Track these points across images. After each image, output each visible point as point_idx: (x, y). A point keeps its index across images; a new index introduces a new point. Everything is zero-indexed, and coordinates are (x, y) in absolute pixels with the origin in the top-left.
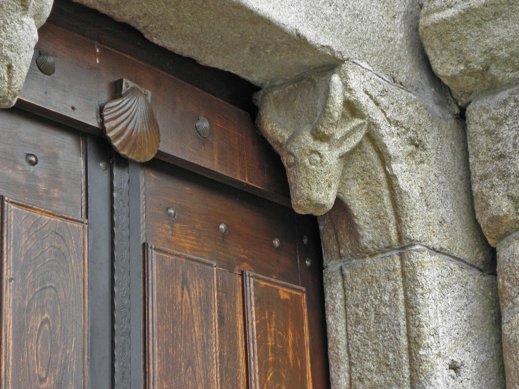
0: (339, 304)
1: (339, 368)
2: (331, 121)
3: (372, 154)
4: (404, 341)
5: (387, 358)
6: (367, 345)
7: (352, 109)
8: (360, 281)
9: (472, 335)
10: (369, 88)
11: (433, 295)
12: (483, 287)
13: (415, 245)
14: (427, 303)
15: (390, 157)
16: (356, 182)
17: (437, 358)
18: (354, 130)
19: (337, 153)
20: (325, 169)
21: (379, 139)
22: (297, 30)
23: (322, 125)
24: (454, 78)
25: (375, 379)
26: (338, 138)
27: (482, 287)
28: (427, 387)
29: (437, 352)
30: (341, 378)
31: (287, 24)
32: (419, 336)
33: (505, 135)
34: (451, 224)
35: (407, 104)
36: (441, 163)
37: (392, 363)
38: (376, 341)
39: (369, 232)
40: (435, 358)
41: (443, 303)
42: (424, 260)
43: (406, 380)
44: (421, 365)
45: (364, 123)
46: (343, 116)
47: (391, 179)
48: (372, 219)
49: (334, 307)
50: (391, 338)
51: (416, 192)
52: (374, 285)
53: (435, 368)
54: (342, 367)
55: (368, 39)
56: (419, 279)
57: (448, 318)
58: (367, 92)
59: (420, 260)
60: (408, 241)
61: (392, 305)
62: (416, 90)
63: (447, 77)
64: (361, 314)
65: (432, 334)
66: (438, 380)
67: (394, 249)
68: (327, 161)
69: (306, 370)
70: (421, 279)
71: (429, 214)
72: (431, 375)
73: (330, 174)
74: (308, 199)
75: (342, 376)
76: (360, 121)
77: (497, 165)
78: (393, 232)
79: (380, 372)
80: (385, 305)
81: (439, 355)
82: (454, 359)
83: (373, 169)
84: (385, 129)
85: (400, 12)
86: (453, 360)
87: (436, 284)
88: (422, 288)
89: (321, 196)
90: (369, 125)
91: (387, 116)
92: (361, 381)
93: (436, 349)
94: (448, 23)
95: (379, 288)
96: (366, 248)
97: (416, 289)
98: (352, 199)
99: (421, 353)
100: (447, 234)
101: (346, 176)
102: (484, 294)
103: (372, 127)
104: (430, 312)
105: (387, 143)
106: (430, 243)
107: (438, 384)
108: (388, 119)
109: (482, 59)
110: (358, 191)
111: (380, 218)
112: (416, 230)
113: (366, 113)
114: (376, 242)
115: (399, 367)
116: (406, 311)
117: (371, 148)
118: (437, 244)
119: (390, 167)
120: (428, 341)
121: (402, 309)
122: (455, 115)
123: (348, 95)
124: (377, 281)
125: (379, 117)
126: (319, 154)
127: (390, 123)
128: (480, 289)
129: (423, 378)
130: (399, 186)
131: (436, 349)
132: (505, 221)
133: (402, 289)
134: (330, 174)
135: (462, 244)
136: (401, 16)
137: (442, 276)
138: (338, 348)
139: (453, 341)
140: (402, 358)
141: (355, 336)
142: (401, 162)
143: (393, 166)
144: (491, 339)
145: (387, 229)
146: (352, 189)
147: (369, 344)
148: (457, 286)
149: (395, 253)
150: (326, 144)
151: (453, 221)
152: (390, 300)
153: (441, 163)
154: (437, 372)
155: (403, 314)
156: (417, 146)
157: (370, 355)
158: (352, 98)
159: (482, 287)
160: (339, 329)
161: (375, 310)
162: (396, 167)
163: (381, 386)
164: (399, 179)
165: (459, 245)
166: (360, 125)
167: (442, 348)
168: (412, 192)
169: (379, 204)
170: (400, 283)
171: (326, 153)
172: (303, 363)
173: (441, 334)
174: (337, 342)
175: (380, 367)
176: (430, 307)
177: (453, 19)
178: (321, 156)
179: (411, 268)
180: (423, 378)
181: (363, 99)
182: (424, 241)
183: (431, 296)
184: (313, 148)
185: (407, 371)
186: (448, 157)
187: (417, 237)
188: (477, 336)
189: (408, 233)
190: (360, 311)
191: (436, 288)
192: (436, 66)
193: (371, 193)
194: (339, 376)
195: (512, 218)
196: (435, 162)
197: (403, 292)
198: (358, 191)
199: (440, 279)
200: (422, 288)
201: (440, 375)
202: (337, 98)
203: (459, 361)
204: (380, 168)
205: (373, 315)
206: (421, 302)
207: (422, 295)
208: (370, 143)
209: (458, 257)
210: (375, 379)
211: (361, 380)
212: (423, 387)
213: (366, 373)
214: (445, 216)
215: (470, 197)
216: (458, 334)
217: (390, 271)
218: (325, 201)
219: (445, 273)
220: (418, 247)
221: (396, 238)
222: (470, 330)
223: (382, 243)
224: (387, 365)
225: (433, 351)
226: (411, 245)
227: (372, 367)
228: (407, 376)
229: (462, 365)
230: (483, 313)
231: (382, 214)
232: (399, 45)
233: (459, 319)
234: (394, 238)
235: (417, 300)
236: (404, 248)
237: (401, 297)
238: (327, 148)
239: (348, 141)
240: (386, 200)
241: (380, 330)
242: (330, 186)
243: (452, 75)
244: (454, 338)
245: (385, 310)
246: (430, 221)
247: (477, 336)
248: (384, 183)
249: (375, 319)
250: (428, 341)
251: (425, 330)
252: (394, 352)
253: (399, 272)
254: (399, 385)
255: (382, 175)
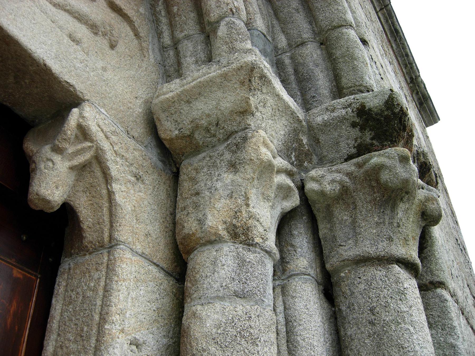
0: (62, 289)
1: (50, 337)
2: (65, 137)
3: (99, 174)
4: (97, 317)
5: (82, 330)
6: (72, 320)
7: (84, 133)
8: (79, 272)
9: (158, 322)
10: (101, 123)
11: (127, 284)
12: (176, 290)
13: (120, 245)
14: (119, 288)
15: (112, 178)
16: (85, 195)
17: (120, 333)
18: (83, 150)
19: (67, 164)
20: (55, 173)
21: (104, 162)
22: (44, 60)
23: (58, 140)
24: (171, 140)
25: (71, 347)
26: (70, 152)
27: (174, 290)
28: (105, 355)
29: (120, 328)
30: (50, 346)
31: (35, 51)
32: (107, 313)
33: (201, 179)
34: (156, 239)
35: (134, 149)
36: (156, 197)
37: (85, 335)
38: (78, 317)
39: (90, 235)
40: (118, 333)
41: (135, 292)
42: (124, 256)
43: (91, 348)
44: (104, 337)
45: (93, 146)
46: (77, 137)
47: (110, 194)
48: (93, 224)
49: (58, 291)
50: (88, 315)
51: (129, 208)
52: (87, 275)
53: (114, 340)
54: (52, 337)
55: (110, 98)
56: (117, 269)
57: (137, 305)
58: (99, 126)
59: (121, 255)
60: (115, 241)
61: (95, 290)
62: (145, 147)
63: (167, 139)
64: (73, 296)
65: (118, 312)
66: (116, 351)
67: (106, 248)
68: (57, 168)
69: (22, 335)
70: (119, 270)
71: (137, 226)
72: (111, 345)
73: (59, 179)
74: (37, 194)
75: (51, 344)
76: (89, 144)
77: (193, 199)
78: (106, 235)
79: (76, 341)
80: (90, 290)
81: (122, 331)
82: (136, 337)
83: (99, 185)
84: (109, 155)
85: (142, 98)
86: (135, 337)
87: (132, 277)
88: (118, 277)
89: (47, 193)
90: (97, 149)
91: (115, 149)
92: (62, 348)
93: (120, 326)
94: (170, 101)
95: (89, 277)
96: (87, 246)
97: (113, 277)
98: (80, 207)
99: (106, 327)
100: (151, 244)
101: (77, 188)
102: (175, 296)
103: (100, 151)
104: (120, 296)
105: (110, 166)
106: (134, 247)
107: (115, 354)
108: (115, 151)
109: (190, 126)
110: (85, 202)
111: (99, 224)
112: (123, 234)
113: (95, 139)
114: (94, 242)
115: (89, 338)
116: (104, 293)
117: (98, 169)
118: (140, 249)
119: (111, 185)
120: (113, 318)
121: (101, 293)
122: (173, 173)
123: (81, 120)
124: (89, 272)
125: (106, 145)
126: (53, 161)
127: (116, 154)
128: (173, 291)
129: (103, 347)
130: (115, 200)
131: (120, 326)
132: (193, 238)
133: (104, 278)
134: (59, 179)
135: (162, 253)
136: (142, 100)
137: (139, 273)
138: (53, 322)
139: (139, 323)
140: (92, 331)
141: (66, 313)
142: (121, 184)
143: (114, 185)
144: (176, 329)
145: (102, 233)
146: (81, 199)
147: (73, 320)
148: (151, 283)
149: (105, 251)
150: (59, 155)
151: (158, 238)
152: (95, 286)
153: (156, 197)
154: (116, 343)
155: (101, 296)
156: (138, 179)
157: (72, 328)
158: (84, 124)
159: (174, 290)
160: (57, 308)
161: (83, 294)
162: (115, 187)
163: (74, 353)
164: (117, 195)
165: (159, 255)
166: (90, 147)
167: (127, 326)
168: (125, 206)
169: (100, 213)
170: (104, 273)
171: (58, 162)
172: (21, 329)
173: (128, 315)
174: (54, 318)
175: (76, 337)
176: (121, 292)
177: (173, 98)
178: (54, 164)
179: (113, 262)
180: (103, 347)
181: (94, 128)
182: (128, 243)
183: (124, 284)
184: (49, 157)
185: (94, 342)
186: (163, 196)
187: (122, 239)
188: (162, 324)
189: (116, 235)
190: (74, 294)
191: (132, 280)
192: (161, 132)
193: (95, 204)
194: (48, 343)
195: (198, 236)
196: (150, 194)
197: (104, 280)
198: (85, 202)
199: (136, 274)
200: (118, 277)
201: (119, 347)
202: (72, 121)
203: (141, 340)
204: (103, 186)
205: (81, 298)
206: (115, 287)
207: (117, 281)
208: (98, 166)
209: (158, 263)
210: (71, 347)
211: (61, 347)
212: (102, 354)
213: (66, 342)
214: (151, 232)
215: (174, 223)
216: (145, 319)
217: (99, 264)
218: (51, 198)
219: (142, 271)
220: (121, 246)
221: (108, 239)
222: (157, 318)
223: (97, 243)
224: (82, 336)
225: (117, 326)
226: (117, 245)
227: (71, 338)
228: (93, 346)
229: (144, 343)
230: (172, 308)
231: (101, 221)
232: (136, 114)
233: (148, 308)
234: (106, 239)
235: (112, 286)
236: (111, 247)
237: (102, 284)
238: (60, 158)
239: (79, 158)
240: (105, 210)
241: (83, 308)
242: (57, 188)
243: (170, 138)
244: (140, 321)
245: (89, 294)
246: (137, 231)
247: (162, 324)
248: (106, 198)
249: (82, 300)
250: (113, 318)
251: (113, 309)
252: (88, 326)
253: (105, 265)
254: (86, 353)
255: (104, 192)
